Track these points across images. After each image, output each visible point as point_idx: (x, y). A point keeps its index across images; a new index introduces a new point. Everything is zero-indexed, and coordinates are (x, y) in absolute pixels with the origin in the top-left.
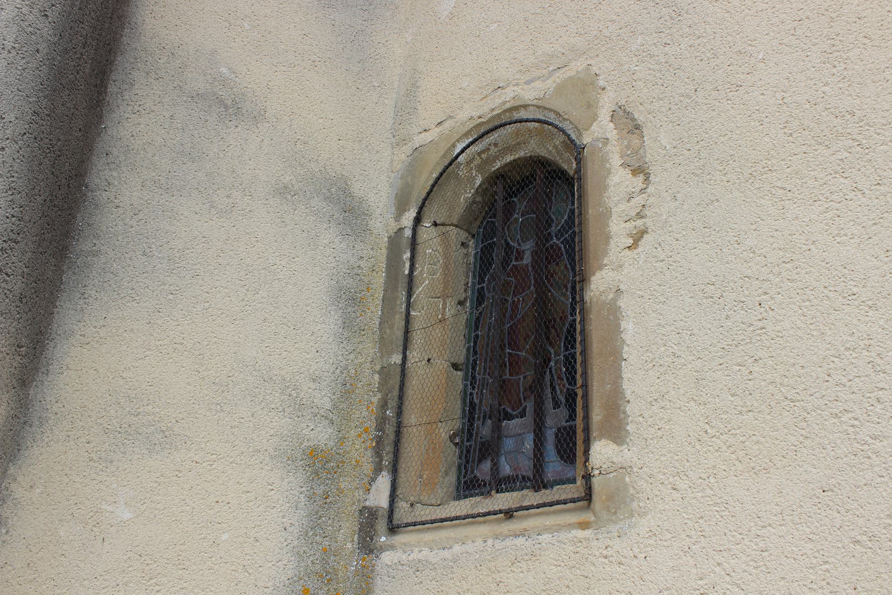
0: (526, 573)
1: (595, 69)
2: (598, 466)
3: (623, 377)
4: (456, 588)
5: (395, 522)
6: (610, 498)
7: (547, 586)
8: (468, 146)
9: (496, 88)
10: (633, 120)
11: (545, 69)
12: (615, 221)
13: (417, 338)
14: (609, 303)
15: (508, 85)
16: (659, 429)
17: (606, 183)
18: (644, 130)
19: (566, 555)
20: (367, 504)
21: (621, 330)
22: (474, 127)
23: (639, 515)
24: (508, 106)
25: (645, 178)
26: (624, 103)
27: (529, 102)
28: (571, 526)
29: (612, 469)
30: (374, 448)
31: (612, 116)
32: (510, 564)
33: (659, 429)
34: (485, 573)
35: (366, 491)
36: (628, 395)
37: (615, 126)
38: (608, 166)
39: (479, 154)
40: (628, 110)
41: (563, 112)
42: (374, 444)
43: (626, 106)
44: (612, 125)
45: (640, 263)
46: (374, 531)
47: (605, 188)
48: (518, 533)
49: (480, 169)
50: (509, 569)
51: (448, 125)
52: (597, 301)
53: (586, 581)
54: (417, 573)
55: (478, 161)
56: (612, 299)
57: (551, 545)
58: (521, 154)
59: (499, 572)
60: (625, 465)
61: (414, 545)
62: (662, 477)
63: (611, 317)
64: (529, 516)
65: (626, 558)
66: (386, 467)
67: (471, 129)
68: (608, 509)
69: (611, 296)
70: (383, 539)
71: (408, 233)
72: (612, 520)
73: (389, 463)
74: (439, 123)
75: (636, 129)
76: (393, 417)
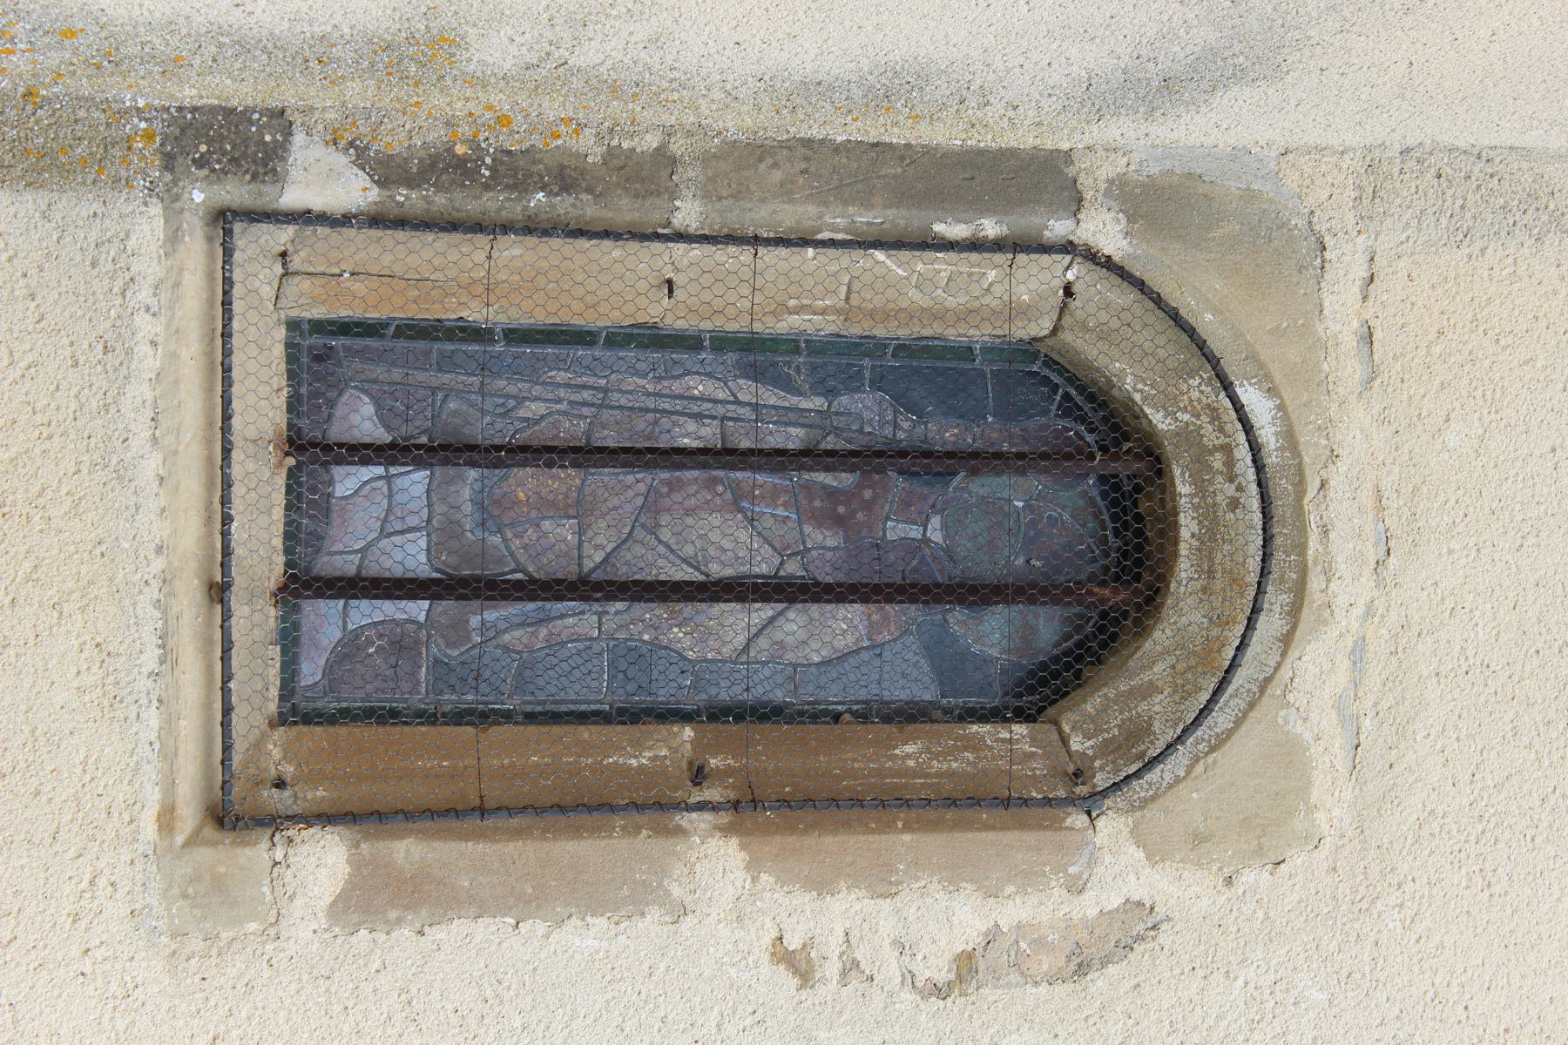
0: (75, 684)
1: (1297, 860)
2: (292, 860)
3: (480, 920)
4: (55, 483)
5: (238, 227)
6: (219, 885)
7: (42, 740)
8: (1255, 449)
9: (1392, 544)
10: (1105, 961)
11: (1376, 704)
12: (857, 907)
13: (735, 258)
14: (660, 884)
15: (1380, 583)
16: (346, 1008)
17: (964, 885)
18: (1069, 987)
19: (106, 786)
20: (299, 138)
21: (588, 919)
22: (1300, 464)
23: (174, 953)
24: (1315, 583)
25: (939, 985)
26: (1161, 940)
27: (1293, 654)
28: (169, 785)
29: (279, 891)
30: (450, 150)
31: (1140, 904)
32: (98, 640)
33: (346, 1008)
34: (84, 569)
35: (335, 131)
36: (438, 933)
37: (1109, 913)
38: (1010, 889)
39: (1227, 450)
40: (1138, 948)
41: (1215, 762)
42: (460, 150)
43: (1151, 945)
44: (1116, 902)
45: (733, 971)
46: (222, 170)
47: (952, 883)
48: (170, 644)
49: (1188, 436)
50: (88, 637)
51: (1347, 368)
52: (675, 853)
53: (46, 835)
54: (100, 347)
55: (1211, 437)
56: (668, 894)
57: (130, 747)
58: (1185, 568)
59: (83, 609)
60: (284, 923)
61: (172, 319)
62: (243, 1014)
63: (625, 891)
64: (207, 656)
65: (87, 929)
66: (390, 197)
67: (1300, 455)
68: (196, 879)
69: (676, 891)
70: (198, 197)
71: (1058, 228)
72: (170, 886)
73: (401, 205)
74: (1371, 335)
75: (1080, 965)
76: (526, 208)
